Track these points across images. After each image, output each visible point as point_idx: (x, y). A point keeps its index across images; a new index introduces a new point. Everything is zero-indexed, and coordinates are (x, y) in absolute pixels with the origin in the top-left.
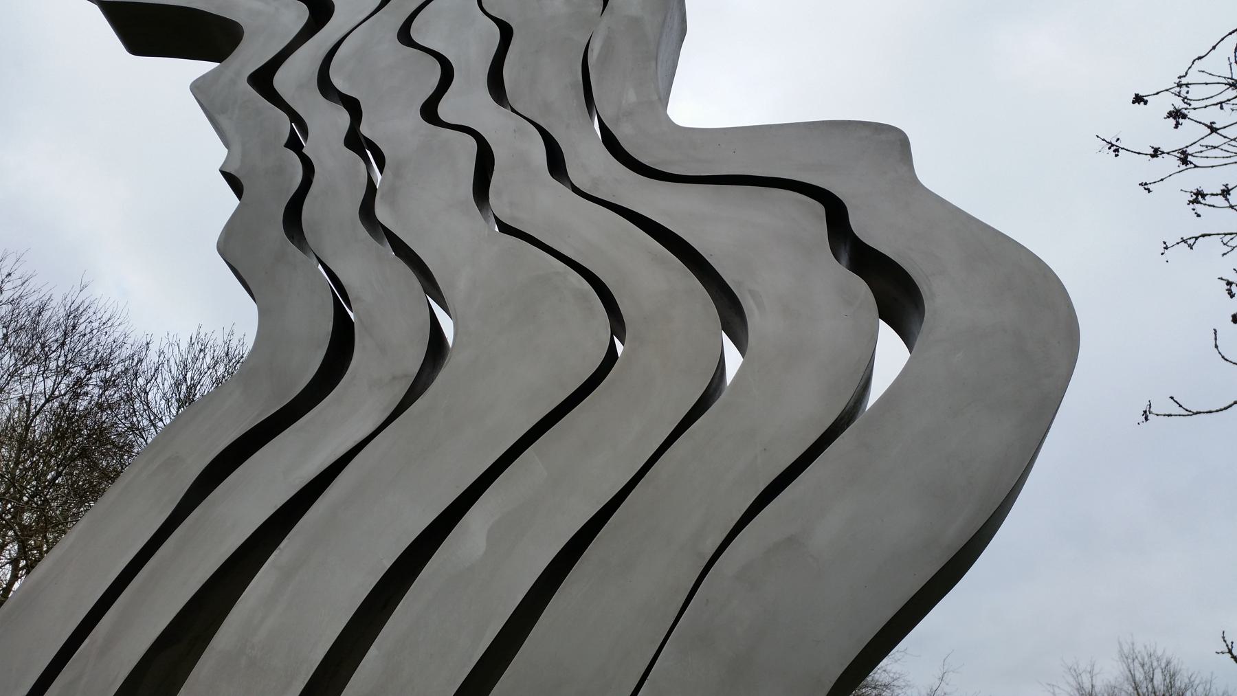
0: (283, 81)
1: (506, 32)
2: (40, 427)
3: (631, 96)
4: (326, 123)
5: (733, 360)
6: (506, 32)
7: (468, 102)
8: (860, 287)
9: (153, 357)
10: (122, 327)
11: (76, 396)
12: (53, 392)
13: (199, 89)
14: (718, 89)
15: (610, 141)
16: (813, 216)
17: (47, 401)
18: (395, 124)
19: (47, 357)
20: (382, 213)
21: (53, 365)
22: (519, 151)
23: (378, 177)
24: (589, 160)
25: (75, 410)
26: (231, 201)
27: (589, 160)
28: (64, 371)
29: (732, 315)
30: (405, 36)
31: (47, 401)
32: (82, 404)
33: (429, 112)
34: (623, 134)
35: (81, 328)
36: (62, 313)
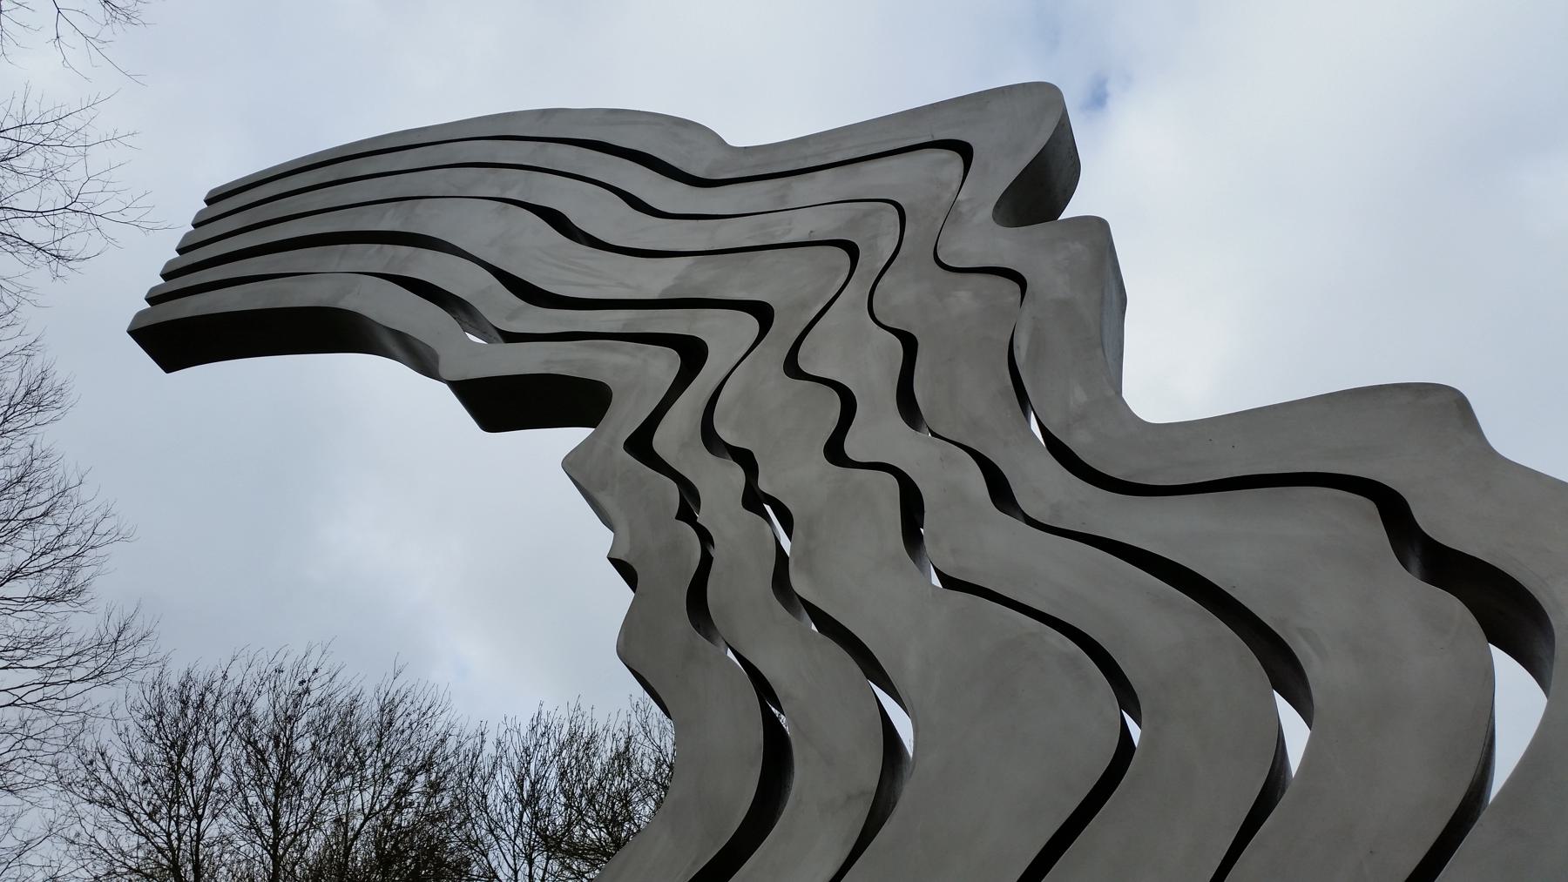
0: (664, 441)
1: (909, 343)
2: (362, 852)
3: (1079, 396)
4: (720, 484)
5: (1296, 734)
6: (909, 343)
7: (878, 433)
8: (1452, 607)
9: (490, 749)
10: (444, 716)
11: (399, 808)
12: (372, 808)
13: (573, 465)
14: (1184, 362)
15: (1057, 448)
16: (1363, 519)
17: (367, 819)
18: (795, 472)
19: (363, 763)
20: (800, 584)
21: (369, 773)
22: (952, 485)
23: (786, 544)
24: (1043, 484)
25: (399, 826)
26: (624, 595)
27: (1043, 484)
28: (385, 776)
29: (1284, 670)
30: (792, 367)
31: (367, 819)
32: (408, 816)
33: (835, 451)
34: (1079, 442)
35: (398, 724)
36: (376, 708)
